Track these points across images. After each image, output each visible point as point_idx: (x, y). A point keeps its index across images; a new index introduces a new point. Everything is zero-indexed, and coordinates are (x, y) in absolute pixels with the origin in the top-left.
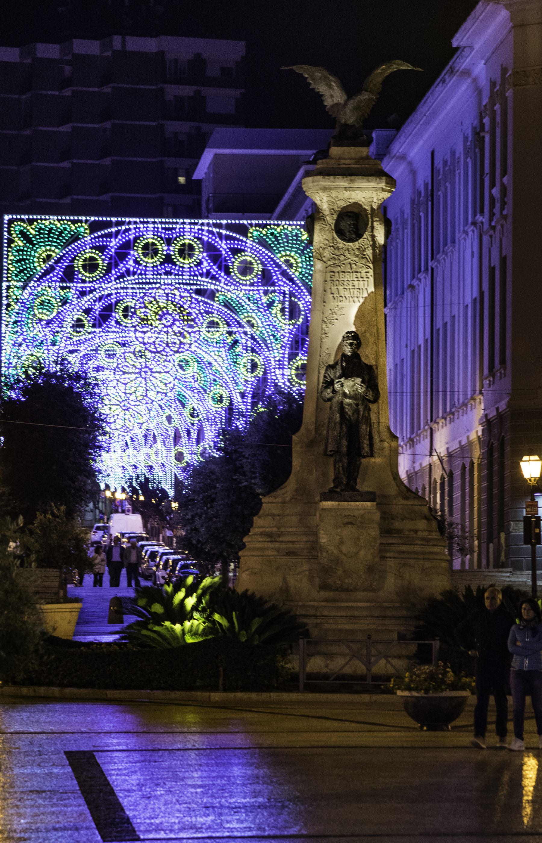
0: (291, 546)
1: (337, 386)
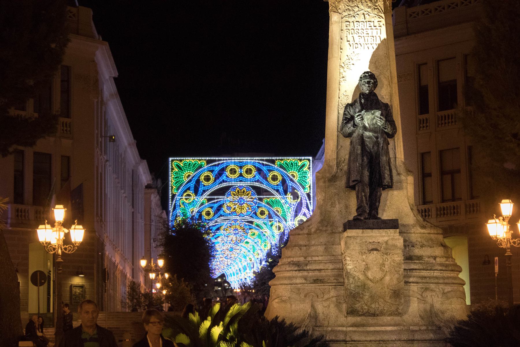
0: (317, 273)
1: (357, 120)
